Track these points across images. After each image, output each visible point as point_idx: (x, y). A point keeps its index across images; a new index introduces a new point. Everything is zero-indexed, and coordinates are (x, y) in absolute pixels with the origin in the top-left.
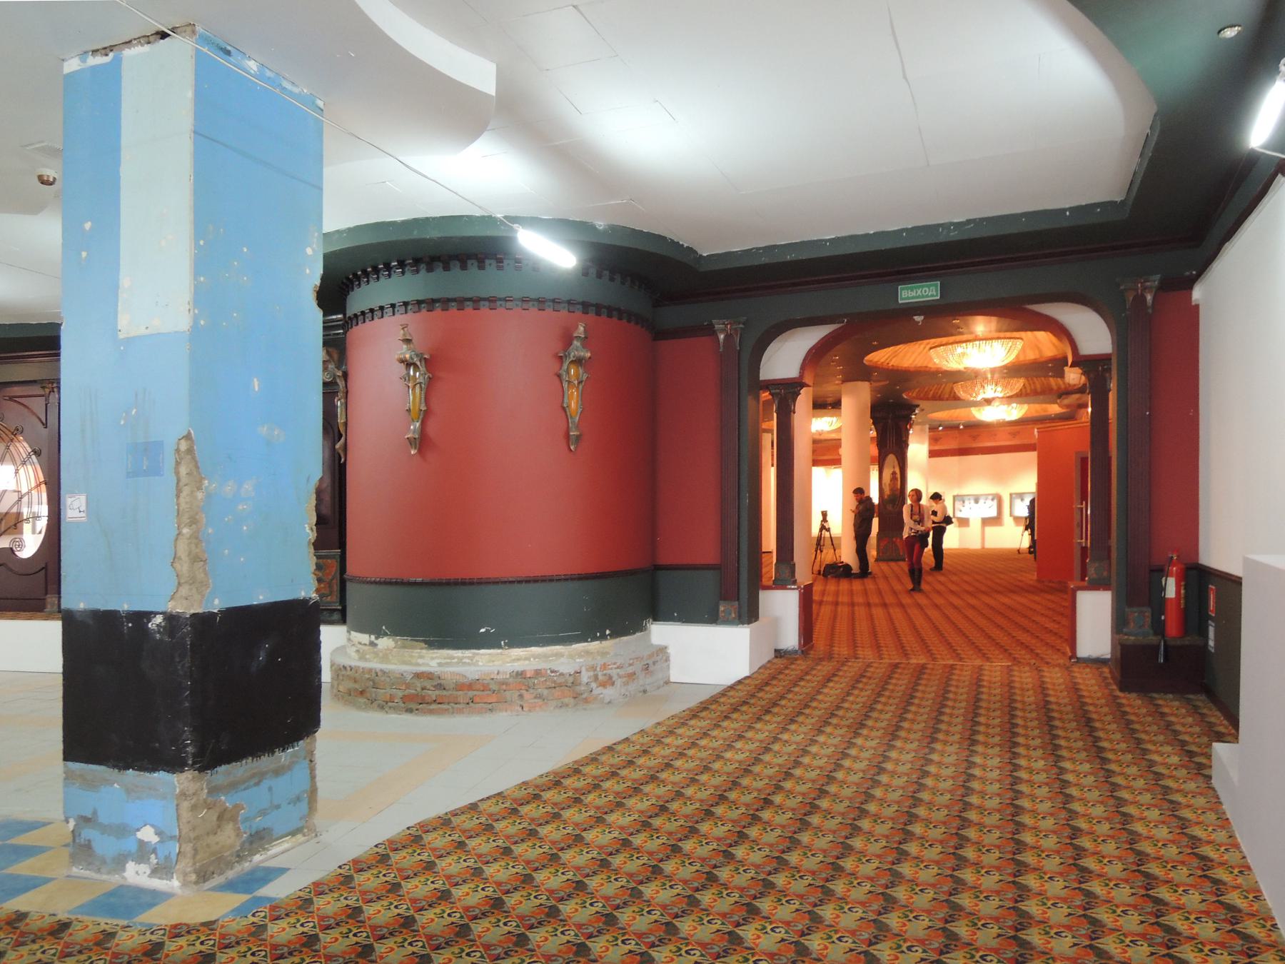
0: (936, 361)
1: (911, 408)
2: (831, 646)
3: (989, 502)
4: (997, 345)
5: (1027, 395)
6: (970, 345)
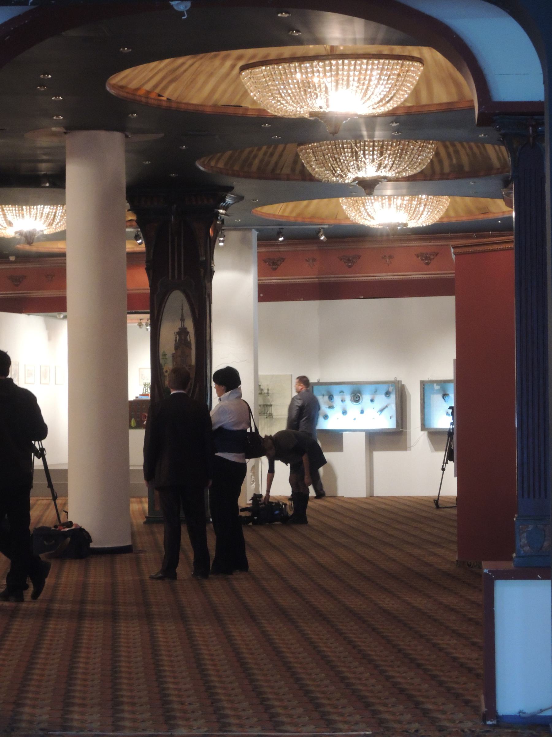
0: (254, 95)
1: (218, 193)
2: (18, 704)
3: (381, 400)
4: (373, 70)
5: (444, 177)
6: (318, 65)
